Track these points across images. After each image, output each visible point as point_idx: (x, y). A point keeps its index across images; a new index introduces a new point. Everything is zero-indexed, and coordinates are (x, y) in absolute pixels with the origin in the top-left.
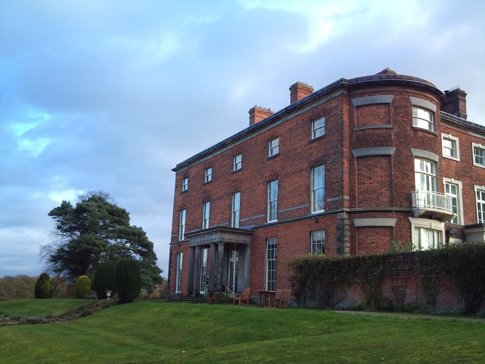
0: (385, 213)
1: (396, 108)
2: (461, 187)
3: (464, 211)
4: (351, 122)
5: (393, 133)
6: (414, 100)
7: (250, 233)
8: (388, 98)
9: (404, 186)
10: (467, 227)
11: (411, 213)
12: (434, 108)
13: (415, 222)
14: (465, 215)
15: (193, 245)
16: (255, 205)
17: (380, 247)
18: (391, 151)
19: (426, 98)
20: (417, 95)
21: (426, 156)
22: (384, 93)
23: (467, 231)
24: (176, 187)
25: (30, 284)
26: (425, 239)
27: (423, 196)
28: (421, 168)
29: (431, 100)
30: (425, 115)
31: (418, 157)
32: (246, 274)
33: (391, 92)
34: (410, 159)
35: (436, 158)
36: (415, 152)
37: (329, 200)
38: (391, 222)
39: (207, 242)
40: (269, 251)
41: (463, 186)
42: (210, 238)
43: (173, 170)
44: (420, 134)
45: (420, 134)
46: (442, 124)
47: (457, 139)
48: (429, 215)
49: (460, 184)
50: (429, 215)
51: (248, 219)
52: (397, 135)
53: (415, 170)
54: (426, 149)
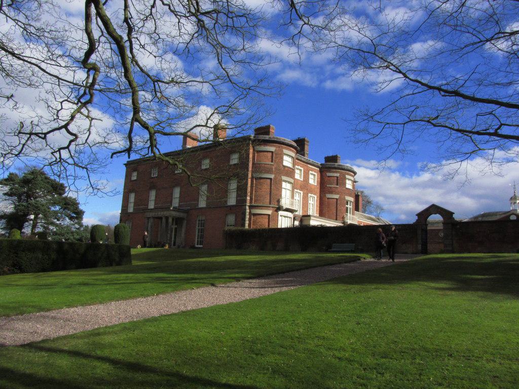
0: (267, 207)
1: (276, 154)
2: (302, 194)
3: (303, 207)
4: (254, 159)
5: (274, 167)
6: (285, 151)
7: (187, 212)
8: (272, 149)
9: (276, 195)
10: (303, 216)
11: (280, 208)
12: (293, 155)
13: (281, 213)
14: (302, 209)
15: (148, 216)
16: (190, 196)
17: (264, 224)
18: (272, 176)
19: (291, 150)
20: (287, 149)
21: (288, 180)
22: (271, 146)
23: (304, 218)
24: (126, 176)
25: (174, 227)
26: (284, 222)
27: (285, 202)
28: (286, 187)
29: (292, 151)
30: (290, 159)
31: (286, 181)
32: (183, 235)
33: (274, 146)
34: (281, 181)
35: (292, 181)
36: (284, 178)
37: (238, 198)
38: (269, 212)
39: (160, 216)
40: (199, 224)
41: (303, 193)
42: (162, 213)
43: (125, 164)
44: (286, 169)
45: (286, 169)
46: (297, 160)
47: (302, 169)
48: (287, 210)
49: (302, 192)
50: (287, 210)
51: (185, 203)
52: (276, 168)
53: (283, 187)
54: (288, 176)
